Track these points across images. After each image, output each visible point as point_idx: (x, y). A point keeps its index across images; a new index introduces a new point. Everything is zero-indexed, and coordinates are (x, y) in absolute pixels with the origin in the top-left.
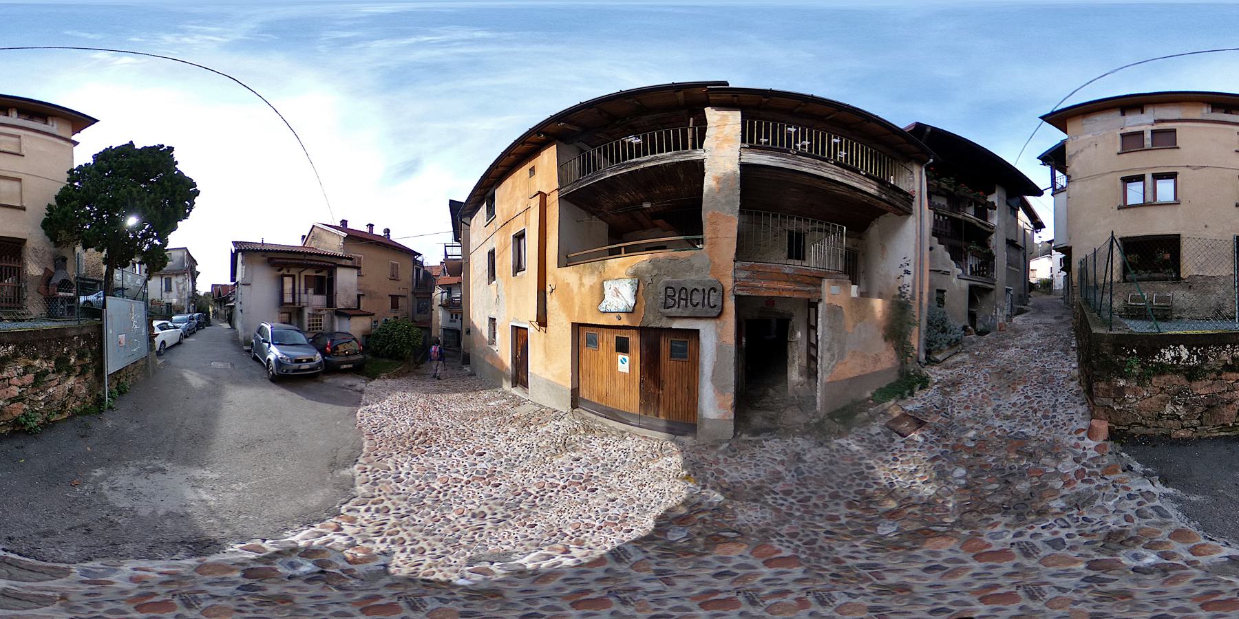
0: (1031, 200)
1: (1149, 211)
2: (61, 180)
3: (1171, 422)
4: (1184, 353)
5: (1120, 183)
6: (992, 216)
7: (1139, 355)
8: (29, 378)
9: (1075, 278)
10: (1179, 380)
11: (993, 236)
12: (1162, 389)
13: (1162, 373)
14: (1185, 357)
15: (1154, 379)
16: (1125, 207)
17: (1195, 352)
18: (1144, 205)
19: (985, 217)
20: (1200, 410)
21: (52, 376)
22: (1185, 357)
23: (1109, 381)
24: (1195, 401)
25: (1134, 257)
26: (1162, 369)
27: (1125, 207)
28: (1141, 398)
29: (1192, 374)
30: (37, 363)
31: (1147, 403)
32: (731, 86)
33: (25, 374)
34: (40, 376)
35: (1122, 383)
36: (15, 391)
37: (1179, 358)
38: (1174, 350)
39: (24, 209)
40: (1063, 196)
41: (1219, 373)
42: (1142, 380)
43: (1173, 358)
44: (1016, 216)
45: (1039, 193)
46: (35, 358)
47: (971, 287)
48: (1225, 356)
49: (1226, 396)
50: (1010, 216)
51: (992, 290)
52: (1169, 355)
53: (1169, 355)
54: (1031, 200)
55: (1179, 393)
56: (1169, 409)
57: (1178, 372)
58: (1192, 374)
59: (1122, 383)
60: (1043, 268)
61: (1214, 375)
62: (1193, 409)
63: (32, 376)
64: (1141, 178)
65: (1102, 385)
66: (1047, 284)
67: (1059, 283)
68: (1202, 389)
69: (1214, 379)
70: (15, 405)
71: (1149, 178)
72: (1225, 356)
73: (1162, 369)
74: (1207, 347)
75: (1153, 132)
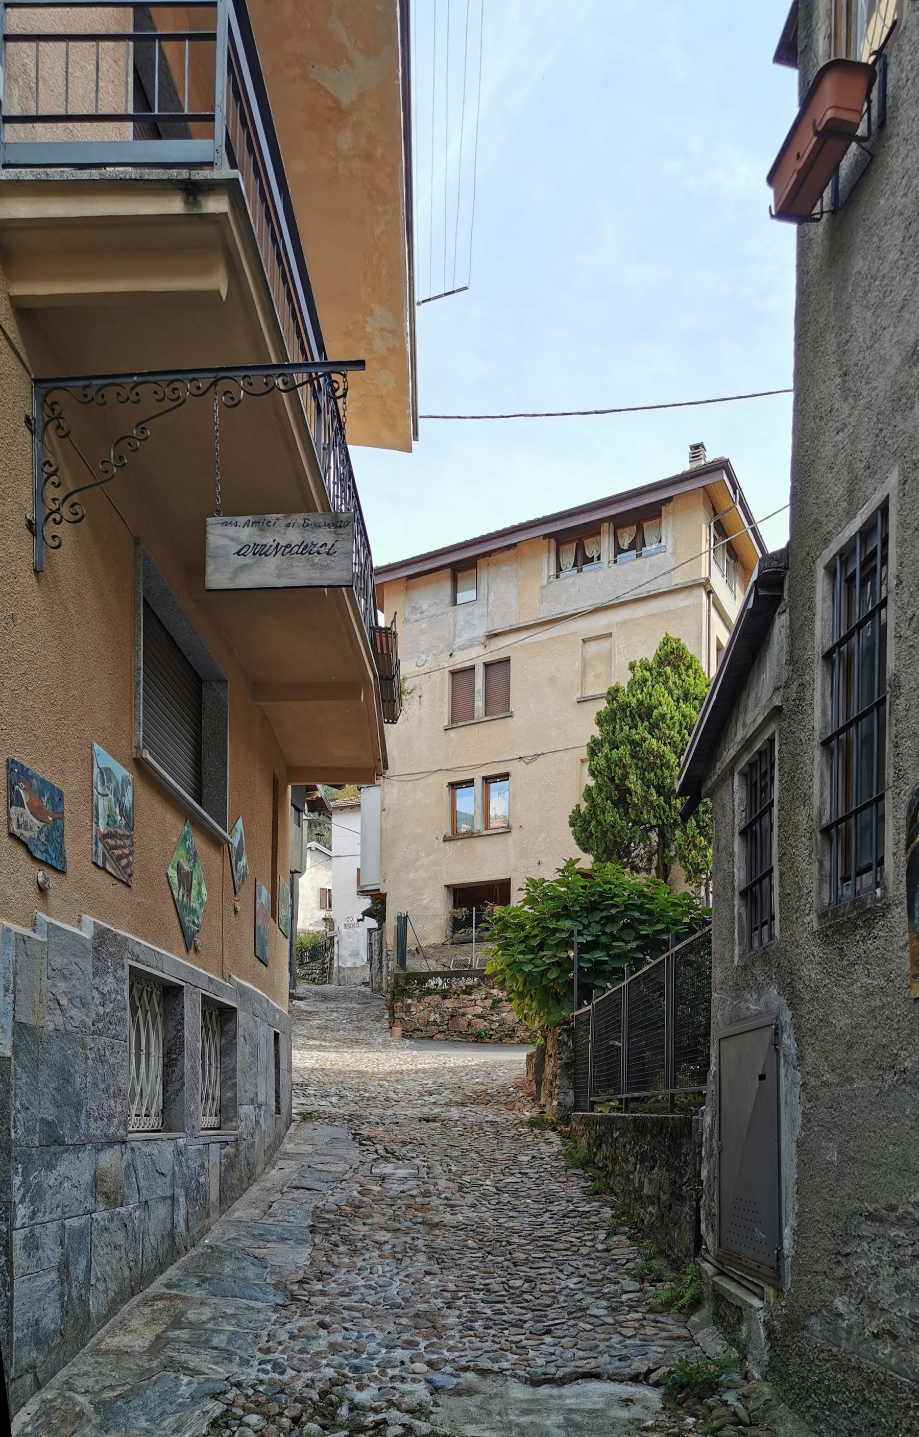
4: (440, 981)
5: (446, 792)
7: (418, 984)
8: (489, 1002)
10: (437, 998)
13: (430, 994)
16: (454, 836)
20: (447, 1018)
21: (505, 1003)
24: (445, 1012)
26: (429, 992)
28: (419, 1010)
29: (445, 995)
30: (495, 991)
31: (422, 1014)
32: (414, 443)
33: (486, 998)
34: (497, 1001)
36: (479, 1010)
39: (63, 873)
46: (493, 988)
48: (461, 983)
59: (410, 1001)
63: (491, 1001)
64: (470, 783)
65: (399, 1004)
68: (449, 1004)
70: (478, 1020)
71: (478, 783)
72: (461, 983)
73: (429, 992)
75: (487, 665)
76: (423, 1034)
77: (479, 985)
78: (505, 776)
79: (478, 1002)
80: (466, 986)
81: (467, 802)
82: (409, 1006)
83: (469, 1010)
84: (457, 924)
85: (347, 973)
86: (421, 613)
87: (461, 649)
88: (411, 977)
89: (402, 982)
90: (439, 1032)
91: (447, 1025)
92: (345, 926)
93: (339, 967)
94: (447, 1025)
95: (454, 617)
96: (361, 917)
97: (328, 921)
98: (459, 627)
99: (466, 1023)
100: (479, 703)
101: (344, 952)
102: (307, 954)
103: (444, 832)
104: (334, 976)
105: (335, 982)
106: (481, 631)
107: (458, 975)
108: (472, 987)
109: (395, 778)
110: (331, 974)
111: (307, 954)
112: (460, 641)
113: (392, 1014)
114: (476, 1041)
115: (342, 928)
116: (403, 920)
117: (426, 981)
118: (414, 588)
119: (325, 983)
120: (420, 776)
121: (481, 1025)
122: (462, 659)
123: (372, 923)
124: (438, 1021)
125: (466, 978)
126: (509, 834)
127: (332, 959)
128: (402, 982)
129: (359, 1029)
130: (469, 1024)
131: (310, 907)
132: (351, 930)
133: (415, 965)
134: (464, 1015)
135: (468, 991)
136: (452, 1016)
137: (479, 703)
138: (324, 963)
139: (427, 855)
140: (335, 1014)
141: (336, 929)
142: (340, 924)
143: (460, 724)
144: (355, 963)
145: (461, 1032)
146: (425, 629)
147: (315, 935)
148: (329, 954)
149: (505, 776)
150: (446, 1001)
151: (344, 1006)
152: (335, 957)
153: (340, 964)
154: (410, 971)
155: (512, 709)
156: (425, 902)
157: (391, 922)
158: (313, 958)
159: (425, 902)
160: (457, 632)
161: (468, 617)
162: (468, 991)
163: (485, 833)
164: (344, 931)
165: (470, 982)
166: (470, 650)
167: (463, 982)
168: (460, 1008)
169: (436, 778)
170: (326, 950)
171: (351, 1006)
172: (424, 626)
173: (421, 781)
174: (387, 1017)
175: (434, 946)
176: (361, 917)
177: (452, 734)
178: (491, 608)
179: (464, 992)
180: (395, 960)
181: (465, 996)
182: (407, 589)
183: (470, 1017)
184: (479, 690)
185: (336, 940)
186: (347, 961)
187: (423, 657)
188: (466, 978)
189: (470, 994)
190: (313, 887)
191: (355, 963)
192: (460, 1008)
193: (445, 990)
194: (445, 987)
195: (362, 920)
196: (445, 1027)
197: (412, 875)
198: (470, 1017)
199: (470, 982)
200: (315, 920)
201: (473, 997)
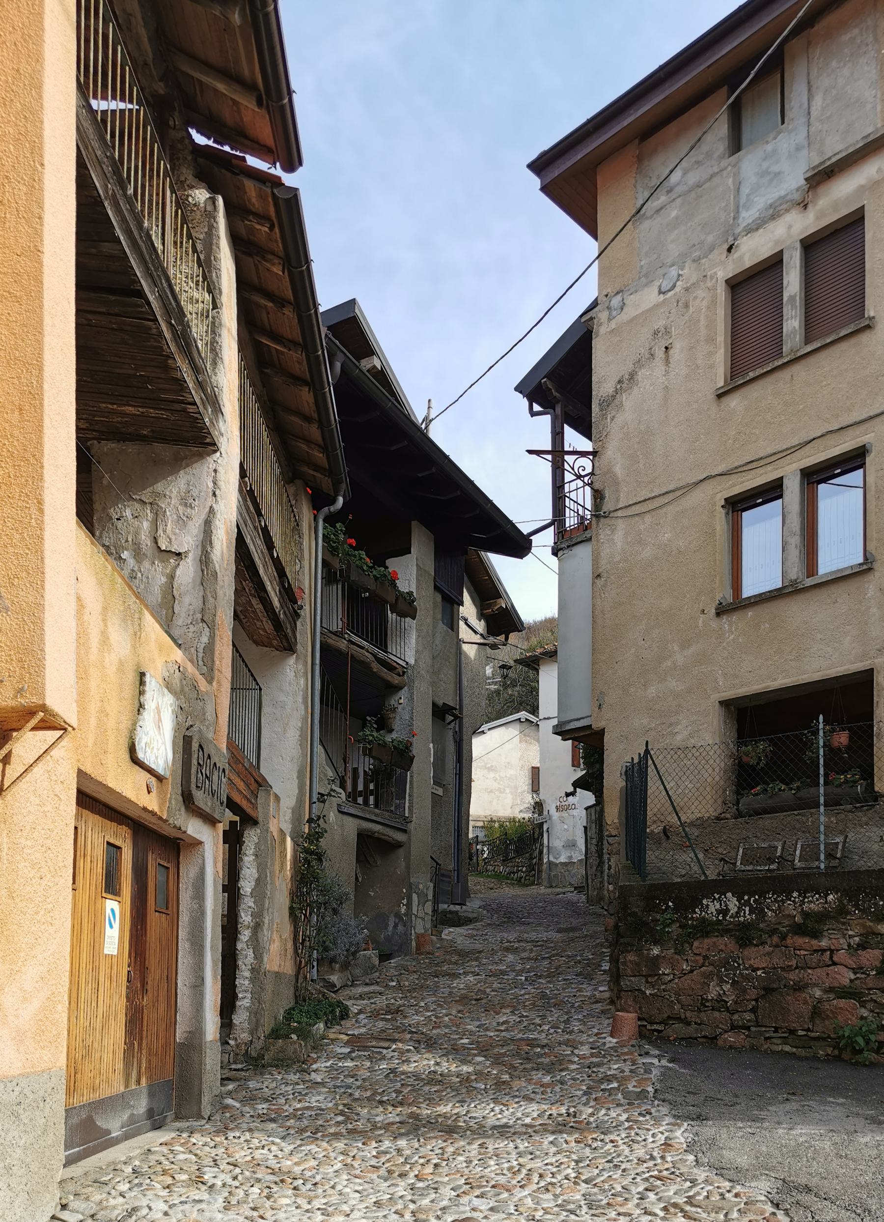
0: (500, 564)
1: (795, 611)
2: (619, 794)
3: (716, 1014)
4: (733, 904)
5: (720, 522)
6: (403, 633)
7: (675, 910)
9: (613, 813)
10: (726, 943)
11: (403, 697)
12: (706, 958)
13: (707, 935)
14: (733, 910)
15: (696, 944)
16: (734, 605)
17: (747, 903)
18: (788, 591)
19: (381, 639)
20: (753, 993)
22: (733, 910)
23: (639, 950)
24: (747, 978)
25: (759, 751)
26: (705, 929)
27: (734, 605)
28: (679, 972)
29: (744, 935)
31: (686, 982)
33: (862, 946)
35: (656, 951)
36: (845, 977)
37: (725, 912)
38: (719, 900)
40: (582, 554)
41: (784, 937)
42: (680, 946)
43: (719, 912)
44: (451, 621)
45: (517, 545)
47: (363, 837)
48: (790, 907)
49: (793, 976)
50: (442, 627)
51: (398, 845)
52: (714, 907)
53: (714, 907)
54: (500, 564)
55: (725, 963)
56: (713, 992)
57: (726, 931)
58: (744, 935)
59: (656, 951)
60: (507, 772)
61: (775, 939)
62: (744, 991)
64: (772, 491)
65: (631, 957)
66: (521, 843)
67: (567, 836)
68: (758, 959)
69: (777, 946)
70: (842, 1003)
71: (793, 488)
72: (790, 907)
73: (705, 929)
74: (763, 894)
76: (691, 1031)
77: (842, 911)
78: (855, 459)
79: (841, 956)
80: (805, 915)
81: (765, 538)
82: (655, 962)
83: (814, 975)
84: (744, 777)
85: (560, 869)
86: (668, 192)
87: (750, 230)
88: (658, 893)
89: (637, 906)
90: (733, 1027)
91: (754, 1010)
92: (557, 808)
93: (550, 863)
94: (754, 1010)
95: (736, 175)
96: (571, 789)
97: (538, 807)
98: (745, 190)
99: (806, 1010)
100: (793, 323)
101: (557, 843)
102: (512, 847)
103: (718, 597)
104: (544, 875)
105: (545, 883)
106: (794, 179)
107: (782, 884)
108: (822, 917)
109: (619, 514)
110: (540, 871)
111: (512, 847)
112: (748, 216)
113: (616, 977)
114: (838, 1059)
115: (553, 811)
116: (637, 774)
117: (696, 902)
118: (654, 152)
119: (533, 884)
120: (665, 499)
121: (851, 1015)
122: (754, 249)
123: (587, 798)
124: (730, 1000)
125: (803, 893)
126: (870, 576)
127: (541, 852)
128: (637, 906)
129: (545, 1003)
130: (816, 1013)
131: (519, 791)
132: (564, 814)
133: (677, 864)
134: (800, 987)
135: (810, 926)
136: (768, 991)
137: (793, 323)
138: (531, 858)
139: (683, 647)
140: (510, 958)
141: (545, 813)
142: (550, 807)
143: (752, 375)
144: (570, 857)
145: (792, 1032)
146: (677, 218)
147: (522, 824)
148: (538, 845)
149: (855, 459)
150: (747, 952)
151: (533, 936)
152: (545, 850)
153: (551, 859)
154: (654, 878)
155: (870, 311)
156: (679, 738)
157: (614, 780)
158: (519, 852)
159: (679, 738)
160: (743, 199)
161: (765, 165)
162: (810, 926)
163: (809, 582)
164: (555, 815)
165: (814, 904)
166: (771, 226)
167: (794, 906)
168: (789, 969)
169: (699, 496)
170: (535, 841)
171: (544, 936)
172: (674, 214)
173: (670, 508)
174: (606, 966)
175: (699, 823)
176: (571, 789)
177: (734, 402)
178: (816, 126)
179: (800, 930)
180: (623, 853)
181: (800, 941)
182: (640, 159)
183: (818, 993)
184: (792, 298)
185: (545, 827)
186: (559, 854)
187: (673, 272)
188: (803, 893)
189: (816, 935)
190: (522, 766)
191: (570, 857)
192: (789, 969)
193: (746, 927)
194: (747, 916)
195: (573, 794)
196: (748, 1016)
197: (652, 691)
198: (818, 993)
199: (814, 904)
200: (526, 805)
201: (824, 943)
